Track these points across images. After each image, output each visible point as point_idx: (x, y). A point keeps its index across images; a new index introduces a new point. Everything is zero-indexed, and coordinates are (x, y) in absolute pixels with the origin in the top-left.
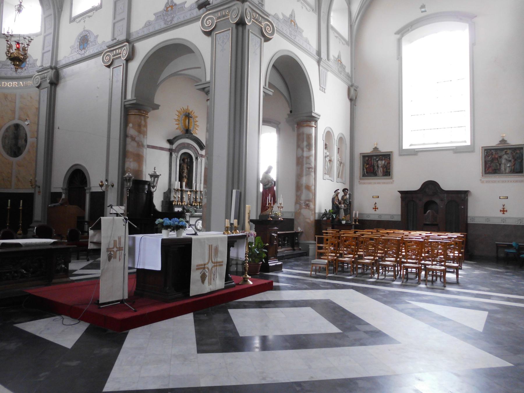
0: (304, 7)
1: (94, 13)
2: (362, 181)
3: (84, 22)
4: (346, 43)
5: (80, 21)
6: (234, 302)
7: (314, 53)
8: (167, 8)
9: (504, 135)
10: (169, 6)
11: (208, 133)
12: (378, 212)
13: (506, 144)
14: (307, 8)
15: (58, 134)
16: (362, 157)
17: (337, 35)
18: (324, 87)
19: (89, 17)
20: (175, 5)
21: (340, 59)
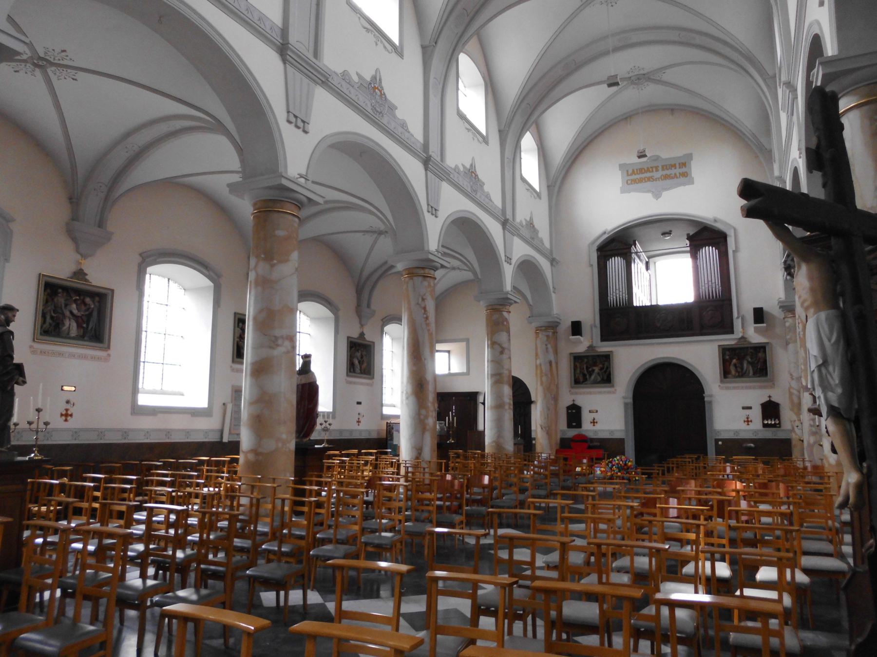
0: (379, 43)
2: (574, 390)
4: (393, 50)
7: (500, 214)
12: (72, 423)
13: (746, 341)
14: (385, 47)
15: (437, 383)
16: (572, 358)
17: (528, 188)
18: (435, 206)
21: (475, 169)
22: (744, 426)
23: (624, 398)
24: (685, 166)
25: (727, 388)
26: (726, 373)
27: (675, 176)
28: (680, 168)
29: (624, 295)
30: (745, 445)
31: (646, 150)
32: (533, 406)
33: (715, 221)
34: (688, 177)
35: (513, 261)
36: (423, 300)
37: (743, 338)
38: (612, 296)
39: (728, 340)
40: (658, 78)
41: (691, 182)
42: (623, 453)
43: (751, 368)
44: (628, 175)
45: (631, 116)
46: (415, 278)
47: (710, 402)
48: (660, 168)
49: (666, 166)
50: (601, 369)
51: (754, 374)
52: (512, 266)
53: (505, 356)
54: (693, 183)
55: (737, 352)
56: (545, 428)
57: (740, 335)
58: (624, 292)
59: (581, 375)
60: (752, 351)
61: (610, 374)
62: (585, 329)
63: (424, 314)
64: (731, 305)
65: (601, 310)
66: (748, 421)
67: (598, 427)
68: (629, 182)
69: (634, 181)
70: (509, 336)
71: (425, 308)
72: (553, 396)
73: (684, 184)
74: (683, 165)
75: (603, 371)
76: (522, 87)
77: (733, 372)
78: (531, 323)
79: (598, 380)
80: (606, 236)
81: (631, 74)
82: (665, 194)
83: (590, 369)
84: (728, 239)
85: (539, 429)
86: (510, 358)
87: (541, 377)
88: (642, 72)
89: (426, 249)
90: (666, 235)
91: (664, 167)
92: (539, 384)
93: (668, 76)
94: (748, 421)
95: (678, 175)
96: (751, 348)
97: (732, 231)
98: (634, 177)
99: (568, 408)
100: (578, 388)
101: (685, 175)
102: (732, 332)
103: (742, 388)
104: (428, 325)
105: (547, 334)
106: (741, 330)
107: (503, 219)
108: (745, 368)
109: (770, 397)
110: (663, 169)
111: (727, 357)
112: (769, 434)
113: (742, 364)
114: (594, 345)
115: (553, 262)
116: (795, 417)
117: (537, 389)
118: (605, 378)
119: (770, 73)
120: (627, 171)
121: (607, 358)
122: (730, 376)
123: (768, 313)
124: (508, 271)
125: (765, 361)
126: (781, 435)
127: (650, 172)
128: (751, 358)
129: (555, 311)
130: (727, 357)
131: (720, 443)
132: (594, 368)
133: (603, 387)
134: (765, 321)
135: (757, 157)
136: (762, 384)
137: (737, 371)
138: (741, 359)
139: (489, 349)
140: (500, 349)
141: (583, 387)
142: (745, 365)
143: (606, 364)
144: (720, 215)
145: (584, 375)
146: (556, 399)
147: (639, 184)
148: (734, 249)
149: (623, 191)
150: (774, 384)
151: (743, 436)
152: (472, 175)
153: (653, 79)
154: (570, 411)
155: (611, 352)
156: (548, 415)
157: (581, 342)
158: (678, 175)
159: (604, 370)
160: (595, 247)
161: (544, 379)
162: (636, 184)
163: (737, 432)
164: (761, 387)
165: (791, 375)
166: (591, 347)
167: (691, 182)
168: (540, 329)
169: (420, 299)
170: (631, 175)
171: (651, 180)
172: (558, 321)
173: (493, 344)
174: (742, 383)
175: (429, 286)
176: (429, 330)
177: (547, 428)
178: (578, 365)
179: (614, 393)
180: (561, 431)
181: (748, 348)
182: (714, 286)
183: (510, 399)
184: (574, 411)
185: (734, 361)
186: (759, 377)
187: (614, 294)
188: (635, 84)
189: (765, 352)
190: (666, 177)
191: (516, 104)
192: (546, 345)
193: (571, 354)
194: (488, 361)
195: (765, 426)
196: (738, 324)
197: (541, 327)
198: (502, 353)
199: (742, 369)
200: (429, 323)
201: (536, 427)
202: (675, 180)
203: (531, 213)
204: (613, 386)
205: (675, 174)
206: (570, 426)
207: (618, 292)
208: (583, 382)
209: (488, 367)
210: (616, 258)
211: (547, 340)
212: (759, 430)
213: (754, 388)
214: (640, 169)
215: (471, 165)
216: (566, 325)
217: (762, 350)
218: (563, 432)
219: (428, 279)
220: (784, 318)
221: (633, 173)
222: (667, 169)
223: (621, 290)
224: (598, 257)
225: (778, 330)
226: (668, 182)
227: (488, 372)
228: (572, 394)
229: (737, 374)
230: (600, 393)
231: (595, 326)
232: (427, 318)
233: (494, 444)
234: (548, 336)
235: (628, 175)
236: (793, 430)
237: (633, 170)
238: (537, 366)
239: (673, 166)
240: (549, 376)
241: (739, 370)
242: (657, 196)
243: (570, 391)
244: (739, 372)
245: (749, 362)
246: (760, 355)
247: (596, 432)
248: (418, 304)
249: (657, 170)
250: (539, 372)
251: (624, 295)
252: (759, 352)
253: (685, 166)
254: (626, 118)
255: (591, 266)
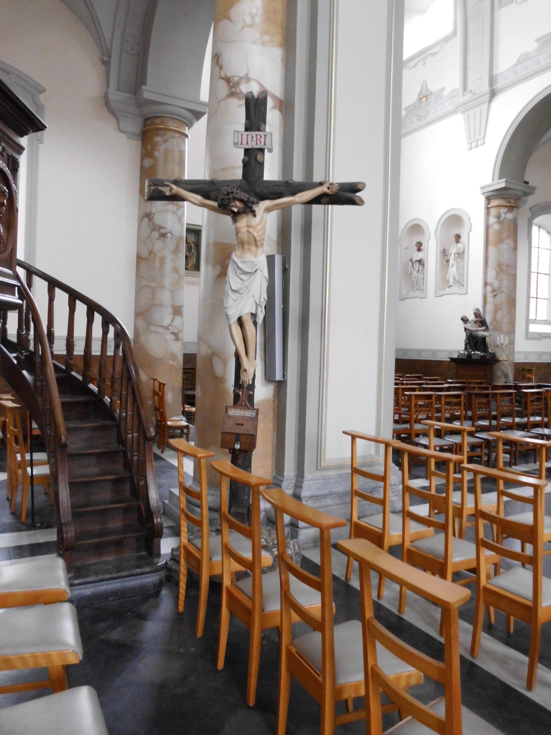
1: (442, 46)
3: (424, 65)
5: (416, 65)
6: (134, 345)
8: (420, 99)
9: (33, 148)
10: (423, 96)
11: (427, 571)
19: (433, 54)
20: (431, 93)
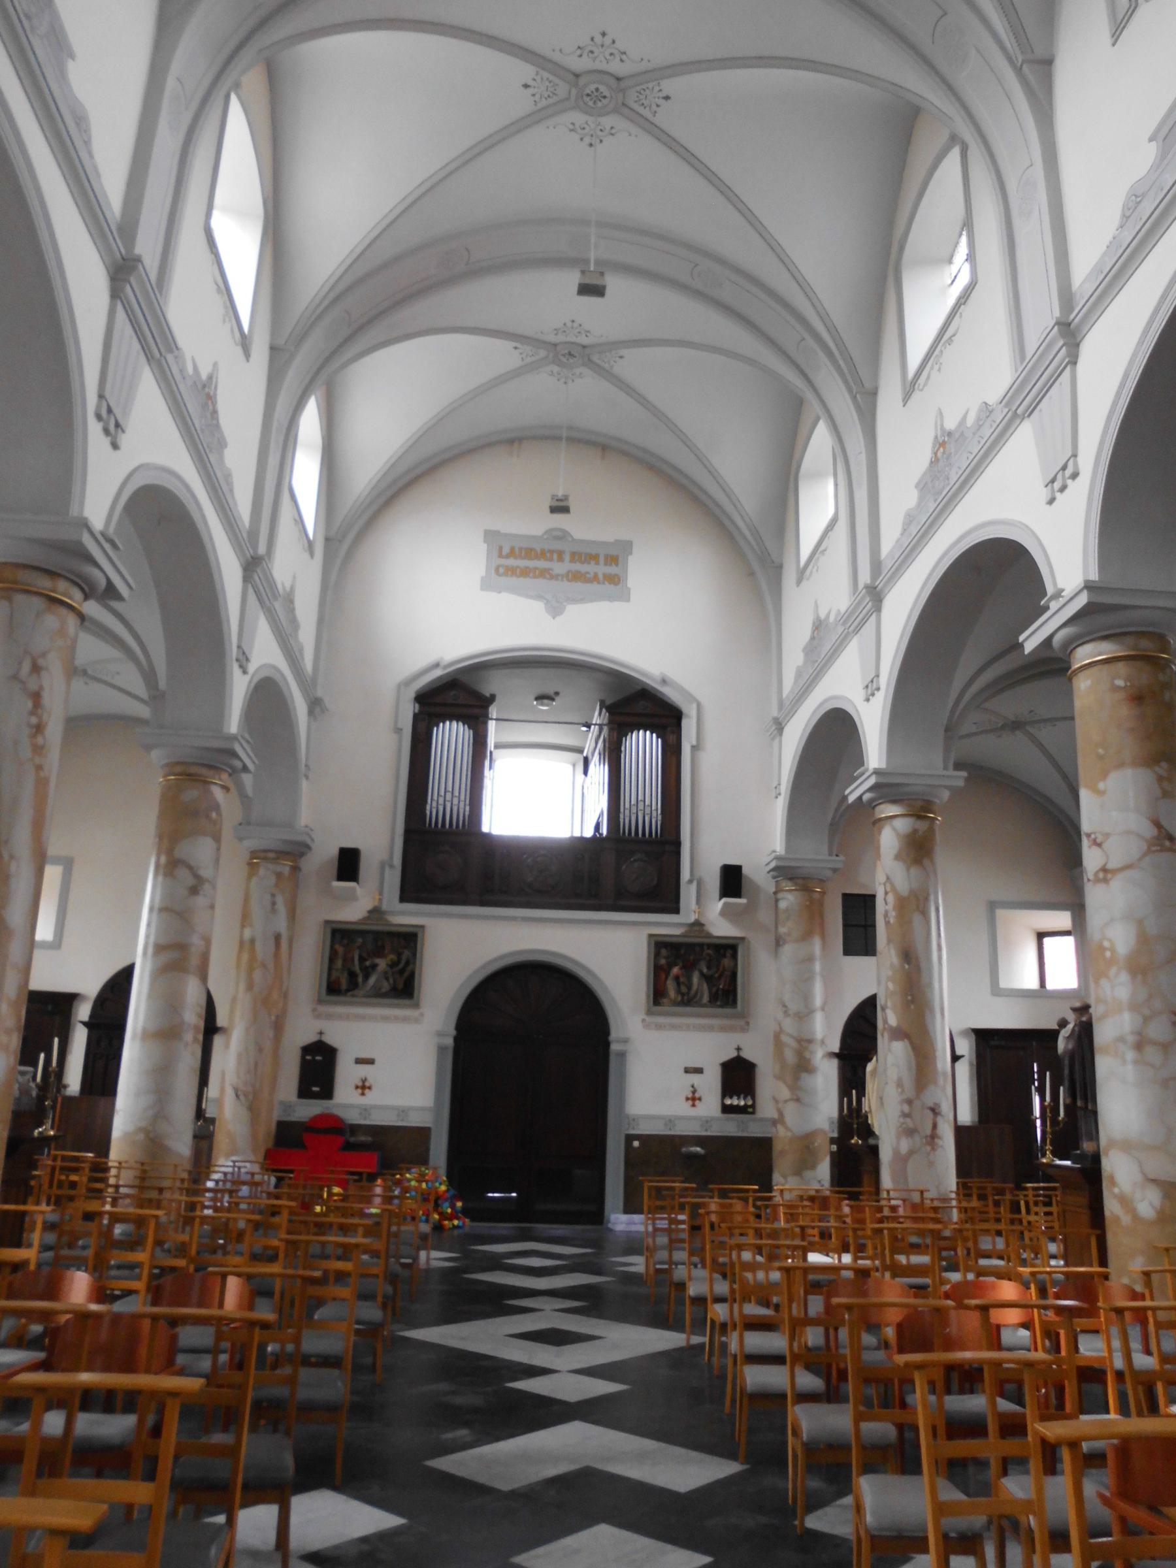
2: (323, 1009)
17: (298, 518)
22: (684, 1109)
23: (440, 1034)
24: (617, 565)
25: (659, 1027)
26: (658, 995)
27: (595, 579)
28: (606, 564)
29: (462, 804)
30: (684, 1150)
31: (571, 499)
32: (835, 1046)
33: (664, 681)
34: (621, 585)
35: (252, 667)
36: (36, 669)
37: (698, 924)
38: (434, 804)
39: (668, 925)
40: (607, 366)
41: (625, 596)
42: (423, 1160)
43: (705, 986)
44: (500, 556)
45: (520, 440)
46: (19, 598)
47: (622, 1055)
48: (567, 557)
49: (580, 554)
50: (393, 965)
51: (710, 1001)
52: (247, 678)
53: (200, 901)
54: (628, 600)
55: (682, 951)
56: (245, 1095)
57: (692, 918)
58: (462, 798)
59: (346, 974)
60: (710, 952)
61: (412, 976)
62: (368, 866)
63: (33, 713)
64: (677, 854)
65: (408, 833)
66: (694, 1099)
67: (370, 1098)
68: (501, 570)
69: (511, 571)
70: (218, 849)
71: (36, 697)
72: (273, 1018)
73: (611, 598)
74: (613, 560)
75: (396, 969)
76: (354, 255)
77: (672, 993)
78: (241, 839)
79: (384, 990)
80: (438, 673)
81: (561, 338)
82: (572, 610)
83: (368, 963)
84: (684, 723)
85: (229, 1096)
86: (212, 907)
87: (251, 970)
88: (583, 340)
89: (74, 511)
90: (546, 701)
91: (575, 557)
92: (242, 986)
93: (629, 366)
94: (694, 1099)
95: (601, 577)
96: (709, 946)
97: (694, 706)
98: (511, 562)
99: (307, 1050)
100: (335, 1003)
101: (615, 580)
102: (677, 911)
103: (688, 1028)
104: (38, 750)
105: (279, 869)
106: (693, 905)
107: (249, 553)
108: (695, 987)
109: (739, 1049)
110: (572, 560)
111: (663, 962)
112: (731, 1127)
113: (689, 978)
114: (384, 907)
115: (315, 705)
116: (785, 1093)
117: (234, 1000)
118: (401, 986)
119: (868, 385)
120: (501, 548)
121: (409, 940)
122: (665, 1000)
123: (751, 881)
124: (239, 687)
125: (734, 975)
126: (753, 1129)
127: (547, 559)
128: (709, 968)
129: (305, 818)
130: (663, 962)
131: (636, 1144)
132: (378, 961)
133: (390, 1006)
134: (744, 891)
135: (752, 574)
136: (726, 1022)
137: (679, 991)
138: (688, 967)
139: (160, 878)
140: (191, 881)
141: (345, 1003)
142: (696, 979)
143: (406, 954)
144: (674, 674)
145: (352, 975)
146: (278, 1027)
147: (521, 579)
148: (694, 743)
149: (486, 585)
150: (748, 1023)
151: (681, 1130)
152: (206, 404)
153: (599, 366)
154: (308, 1058)
155: (422, 927)
156: (256, 1064)
157: (353, 897)
158: (601, 577)
159: (401, 965)
160: (411, 693)
161: (257, 975)
162: (514, 579)
163: (670, 1121)
164: (723, 1029)
165: (784, 1006)
166: (376, 912)
167: (625, 596)
168: (262, 855)
169: (26, 667)
170: (507, 556)
171: (548, 576)
172: (309, 842)
173: (171, 866)
174: (688, 1019)
175: (62, 632)
176: (39, 768)
177: (251, 1097)
178: (340, 949)
179: (417, 1021)
180: (281, 1103)
181: (701, 945)
182: (648, 811)
183: (199, 1016)
184: (319, 1058)
185: (676, 970)
186: (722, 1006)
187: (441, 801)
188: (560, 364)
189: (734, 956)
190: (576, 577)
191: (325, 297)
192: (273, 895)
193: (327, 922)
194: (151, 909)
195: (726, 1109)
196: (688, 894)
197: (265, 851)
198: (194, 891)
199: (689, 987)
200: (42, 747)
201: (222, 1090)
202: (594, 587)
203: (294, 578)
204: (417, 1006)
205: (596, 575)
206: (304, 1092)
207: (449, 796)
208: (348, 990)
209: (149, 925)
210: (454, 724)
211: (277, 885)
212: (713, 1119)
213: (711, 1028)
214: (526, 549)
215: (210, 377)
216: (326, 851)
217: (729, 953)
218: (287, 1107)
219: (63, 611)
220: (775, 893)
221: (512, 553)
222: (583, 563)
223: (456, 793)
224: (416, 717)
225: (764, 915)
226: (579, 586)
227: (147, 936)
228: (318, 1016)
229: (679, 998)
230: (385, 1018)
231: (392, 866)
232: (39, 728)
233: (141, 1136)
234: (279, 875)
235: (500, 556)
236: (779, 1120)
237: (512, 549)
238: (242, 943)
239: (593, 558)
240: (271, 966)
241: (684, 989)
242: (555, 610)
243: (314, 1010)
244: (683, 995)
245: (702, 974)
246: (726, 962)
247: (365, 1110)
248: (15, 677)
249: (561, 559)
250: (245, 957)
251: (462, 804)
252: (724, 956)
253: (617, 565)
254: (511, 442)
255: (398, 731)
